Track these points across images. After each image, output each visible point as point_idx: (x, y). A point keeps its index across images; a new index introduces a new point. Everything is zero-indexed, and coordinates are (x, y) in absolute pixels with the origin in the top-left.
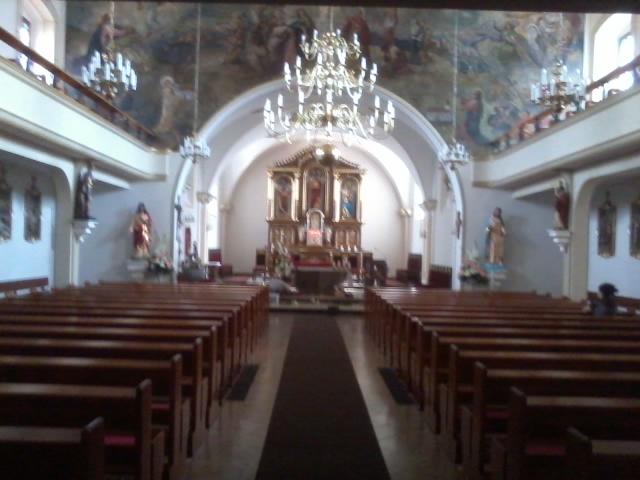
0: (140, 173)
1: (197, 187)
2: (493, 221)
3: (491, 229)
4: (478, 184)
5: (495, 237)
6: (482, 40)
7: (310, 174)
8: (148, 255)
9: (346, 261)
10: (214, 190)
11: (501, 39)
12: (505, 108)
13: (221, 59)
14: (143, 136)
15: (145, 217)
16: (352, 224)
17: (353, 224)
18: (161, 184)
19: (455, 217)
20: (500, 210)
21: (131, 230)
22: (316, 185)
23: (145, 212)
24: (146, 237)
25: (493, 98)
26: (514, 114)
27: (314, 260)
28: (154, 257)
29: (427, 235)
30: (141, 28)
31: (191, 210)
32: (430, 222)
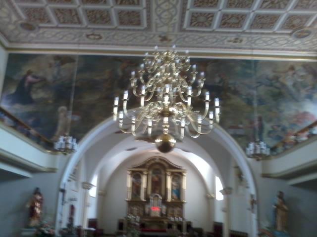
0: (36, 166)
1: (82, 179)
2: (277, 201)
3: (278, 207)
4: (266, 176)
5: (280, 212)
6: (260, 86)
7: (154, 173)
8: (38, 225)
9: (175, 227)
10: (95, 181)
11: (271, 85)
12: (279, 126)
13: (97, 96)
14: (42, 142)
15: (39, 197)
16: (178, 203)
17: (178, 203)
18: (53, 174)
19: (248, 199)
20: (281, 193)
21: (28, 206)
22: (156, 179)
23: (40, 194)
24: (38, 211)
25: (270, 121)
26: (284, 130)
27: (155, 227)
28: (42, 226)
29: (227, 210)
30: (49, 78)
31: (72, 190)
32: (228, 201)
